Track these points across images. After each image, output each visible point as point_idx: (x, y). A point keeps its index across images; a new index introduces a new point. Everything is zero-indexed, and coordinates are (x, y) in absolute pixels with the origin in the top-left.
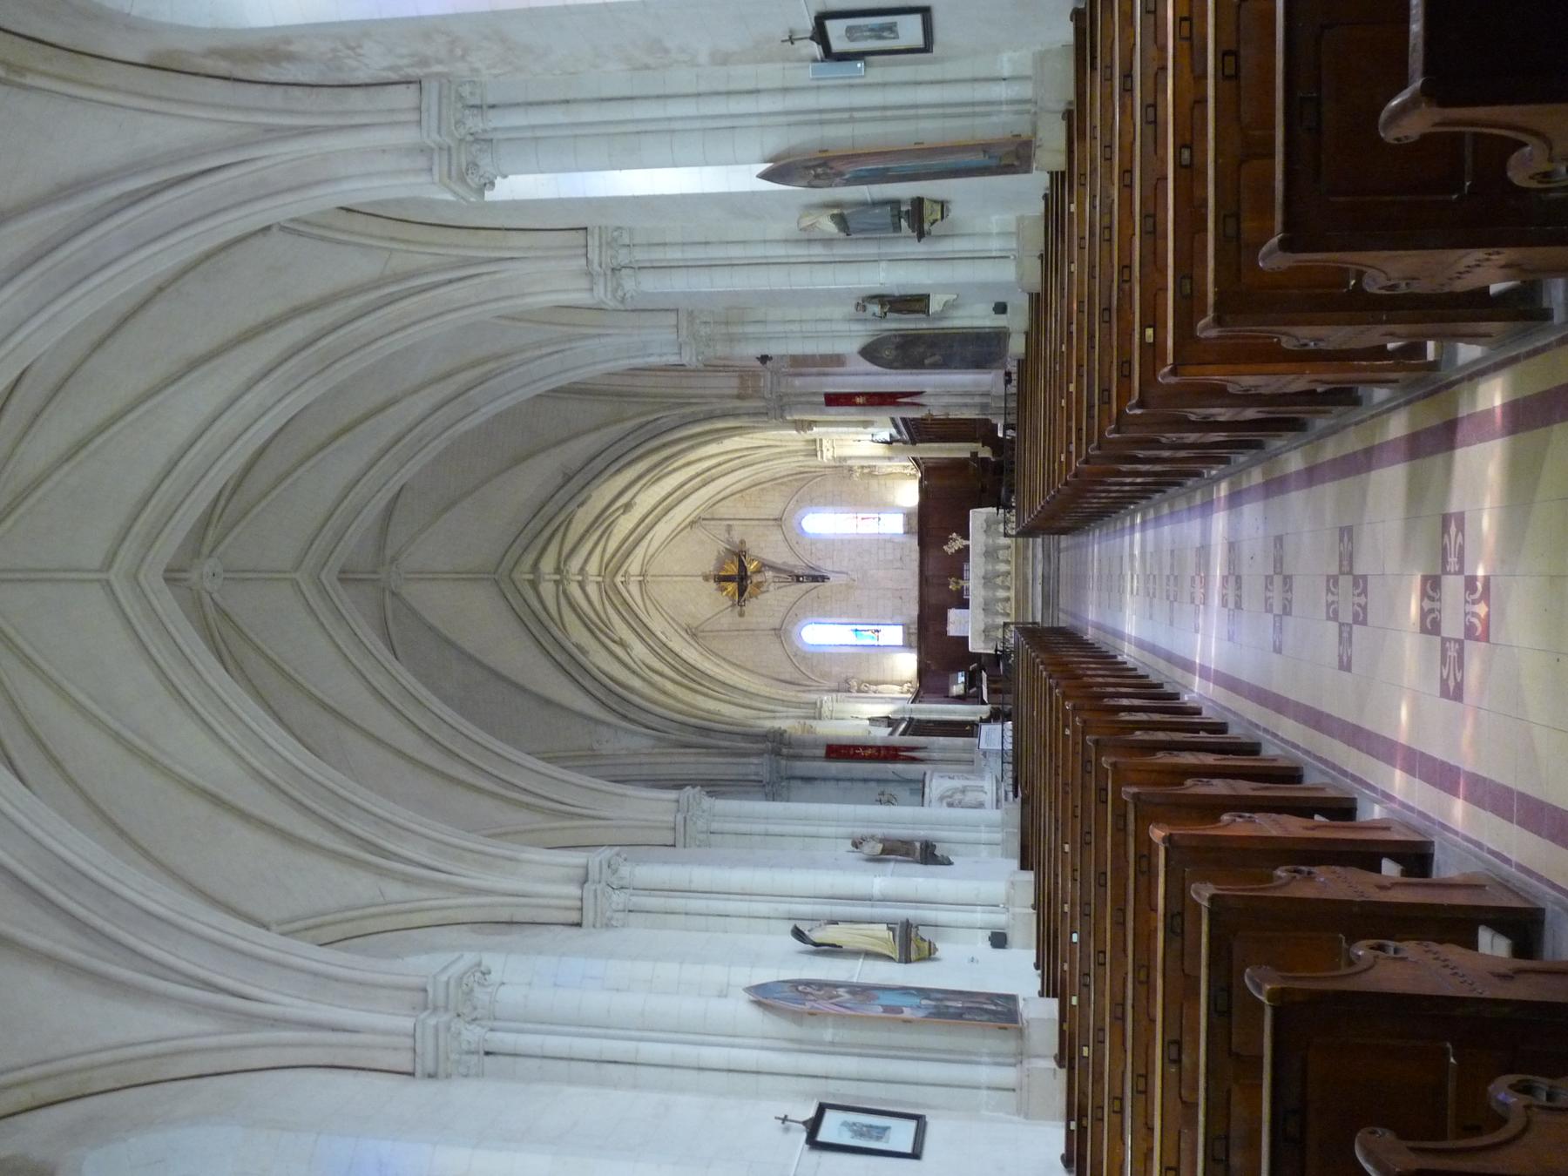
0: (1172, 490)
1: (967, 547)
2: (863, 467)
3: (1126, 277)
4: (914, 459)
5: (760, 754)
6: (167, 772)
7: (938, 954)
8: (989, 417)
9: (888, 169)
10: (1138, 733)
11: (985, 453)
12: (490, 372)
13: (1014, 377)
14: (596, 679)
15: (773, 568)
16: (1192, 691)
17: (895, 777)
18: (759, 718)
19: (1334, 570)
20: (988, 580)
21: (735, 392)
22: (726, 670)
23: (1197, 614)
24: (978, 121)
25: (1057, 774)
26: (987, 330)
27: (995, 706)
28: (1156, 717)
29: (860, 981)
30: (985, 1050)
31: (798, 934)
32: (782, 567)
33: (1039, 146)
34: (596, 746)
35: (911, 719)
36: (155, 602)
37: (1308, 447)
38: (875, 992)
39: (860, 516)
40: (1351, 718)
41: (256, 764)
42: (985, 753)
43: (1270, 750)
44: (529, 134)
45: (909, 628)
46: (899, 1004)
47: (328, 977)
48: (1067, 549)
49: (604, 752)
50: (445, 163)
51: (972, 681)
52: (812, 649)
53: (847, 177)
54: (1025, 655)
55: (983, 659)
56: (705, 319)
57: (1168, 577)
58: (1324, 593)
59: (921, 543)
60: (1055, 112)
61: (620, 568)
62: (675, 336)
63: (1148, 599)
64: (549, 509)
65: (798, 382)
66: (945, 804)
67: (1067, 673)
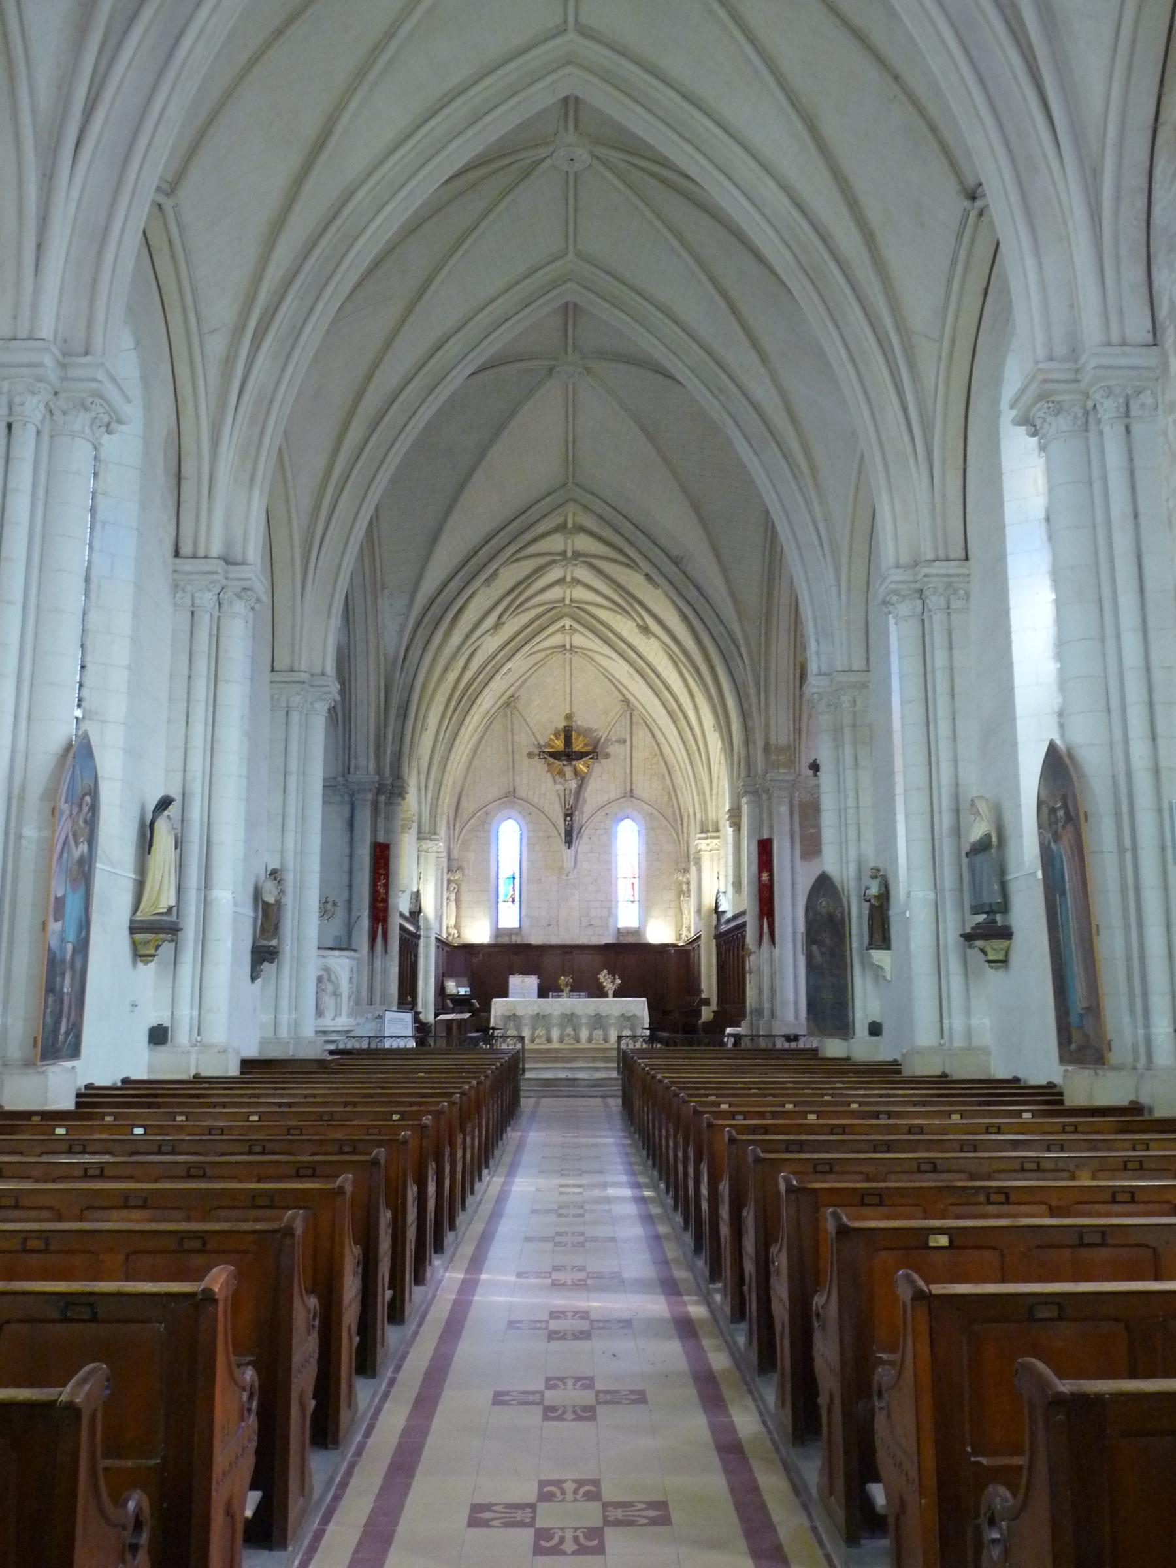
0: (688, 1238)
1: (605, 995)
2: (688, 883)
3: (994, 1198)
4: (699, 937)
5: (379, 771)
6: (351, 89)
7: (140, 965)
8: (748, 1018)
9: (1063, 893)
10: (389, 1214)
11: (707, 1014)
12: (799, 467)
13: (793, 1045)
14: (459, 594)
15: (580, 788)
16: (446, 1269)
17: (354, 918)
18: (419, 773)
19: (609, 1493)
20: (570, 1019)
21: (773, 741)
22: (470, 740)
23: (539, 1275)
24: (1124, 1001)
25: (346, 1104)
26: (851, 1015)
27: (433, 1028)
28: (411, 1233)
29: (97, 870)
30: (10, 1021)
31: (165, 803)
32: (581, 800)
33: (1096, 1074)
34: (386, 592)
35: (418, 937)
36: (540, 85)
37: (769, 1443)
38: (82, 889)
39: (636, 881)
40: (403, 1530)
41: (361, 194)
42: (380, 1017)
43: (364, 1391)
44: (1096, 473)
45: (517, 934)
46: (67, 916)
47: (104, 241)
48: (606, 1105)
49: (379, 601)
50: (1061, 376)
51: (460, 1003)
52: (493, 832)
53: (1053, 846)
54: (488, 1062)
55: (485, 1014)
56: (858, 702)
57: (582, 1234)
58: (576, 1476)
59: (607, 947)
60: (1137, 1091)
61: (579, 622)
62: (840, 669)
63: (555, 1207)
64: (642, 541)
65: (784, 809)
66: (321, 973)
67: (468, 1113)
